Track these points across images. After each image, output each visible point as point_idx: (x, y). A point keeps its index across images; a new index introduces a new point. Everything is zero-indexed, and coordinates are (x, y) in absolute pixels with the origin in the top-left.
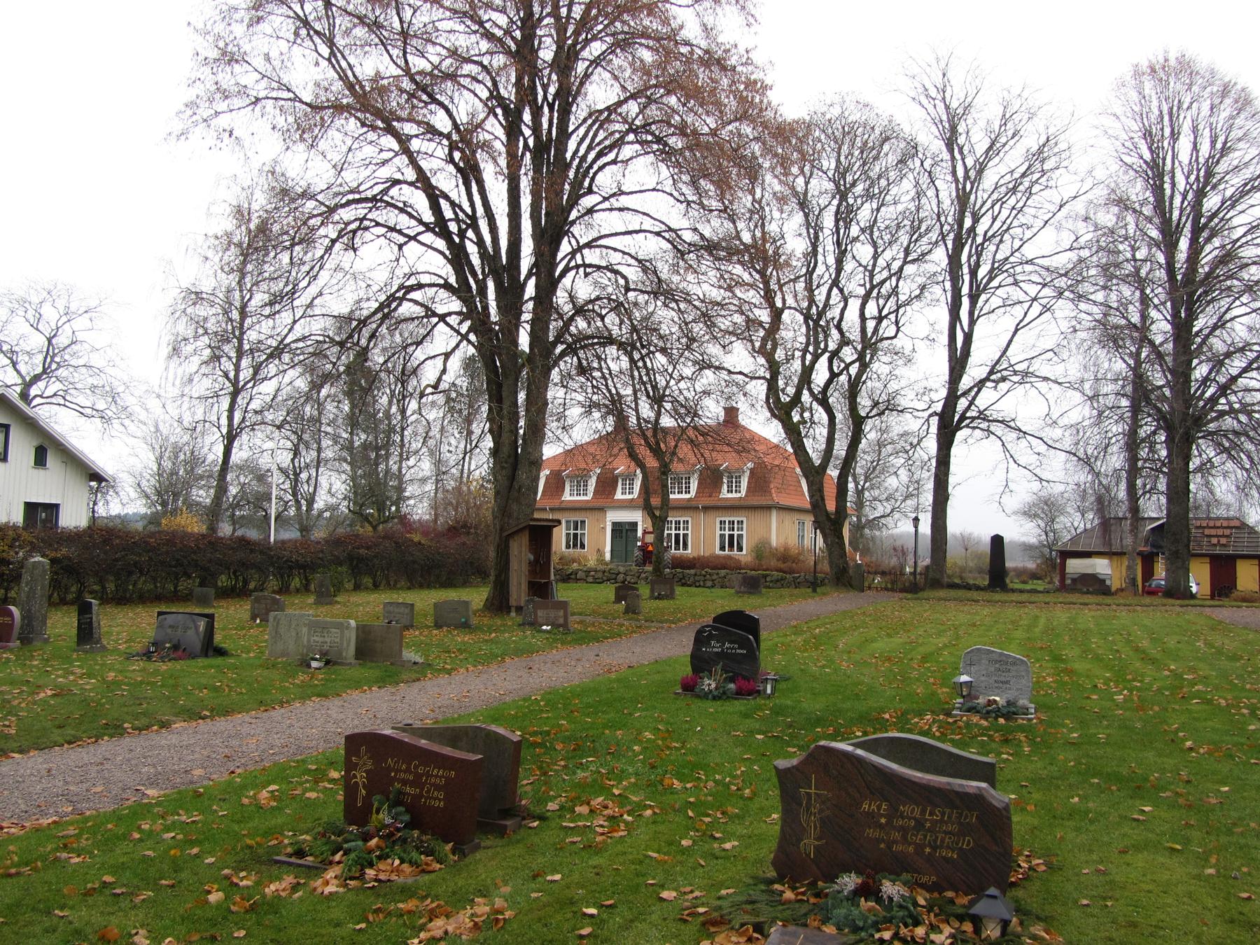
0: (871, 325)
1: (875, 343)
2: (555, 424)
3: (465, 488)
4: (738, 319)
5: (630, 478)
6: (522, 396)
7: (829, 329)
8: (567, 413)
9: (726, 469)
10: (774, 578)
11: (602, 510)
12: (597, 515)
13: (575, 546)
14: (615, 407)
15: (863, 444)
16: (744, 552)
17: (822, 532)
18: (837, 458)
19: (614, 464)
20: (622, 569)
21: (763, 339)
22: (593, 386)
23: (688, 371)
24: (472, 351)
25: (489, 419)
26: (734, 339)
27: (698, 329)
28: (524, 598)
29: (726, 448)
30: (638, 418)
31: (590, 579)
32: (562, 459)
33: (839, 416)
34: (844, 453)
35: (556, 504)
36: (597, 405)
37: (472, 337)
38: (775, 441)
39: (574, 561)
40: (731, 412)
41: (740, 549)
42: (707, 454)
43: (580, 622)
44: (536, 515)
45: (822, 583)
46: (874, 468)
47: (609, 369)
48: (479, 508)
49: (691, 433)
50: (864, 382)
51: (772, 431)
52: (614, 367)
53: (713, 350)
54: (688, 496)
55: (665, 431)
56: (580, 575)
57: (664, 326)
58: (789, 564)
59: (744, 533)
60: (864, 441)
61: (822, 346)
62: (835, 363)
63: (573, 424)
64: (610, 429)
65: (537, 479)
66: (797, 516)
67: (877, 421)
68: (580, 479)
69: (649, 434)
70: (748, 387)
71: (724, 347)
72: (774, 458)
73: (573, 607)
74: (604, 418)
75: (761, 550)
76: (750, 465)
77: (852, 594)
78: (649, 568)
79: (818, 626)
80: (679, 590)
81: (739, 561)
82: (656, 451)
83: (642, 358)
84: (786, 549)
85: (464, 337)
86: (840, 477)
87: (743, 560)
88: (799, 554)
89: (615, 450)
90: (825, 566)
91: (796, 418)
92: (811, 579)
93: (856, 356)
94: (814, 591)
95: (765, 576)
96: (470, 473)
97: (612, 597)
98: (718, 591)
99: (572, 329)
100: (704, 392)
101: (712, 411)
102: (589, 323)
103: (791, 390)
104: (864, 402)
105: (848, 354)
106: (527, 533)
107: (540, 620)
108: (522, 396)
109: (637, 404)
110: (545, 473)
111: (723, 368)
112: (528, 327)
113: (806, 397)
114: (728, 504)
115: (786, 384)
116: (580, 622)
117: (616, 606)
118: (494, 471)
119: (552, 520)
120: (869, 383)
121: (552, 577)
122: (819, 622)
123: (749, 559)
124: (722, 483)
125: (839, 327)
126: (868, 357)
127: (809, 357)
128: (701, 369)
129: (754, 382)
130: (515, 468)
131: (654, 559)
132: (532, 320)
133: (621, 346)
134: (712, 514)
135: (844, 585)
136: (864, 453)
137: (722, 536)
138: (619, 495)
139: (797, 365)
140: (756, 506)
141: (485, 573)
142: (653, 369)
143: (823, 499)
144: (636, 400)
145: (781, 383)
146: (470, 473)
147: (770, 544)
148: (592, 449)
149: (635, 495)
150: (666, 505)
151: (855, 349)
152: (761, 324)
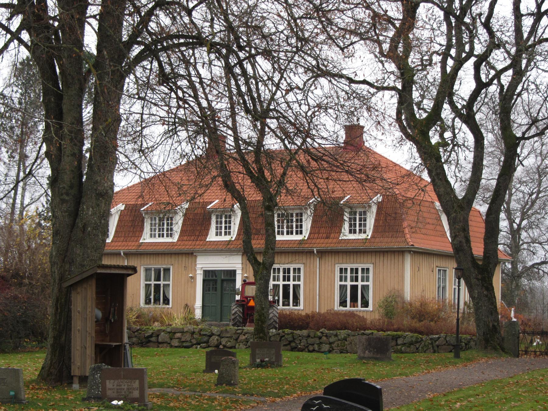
0: (527, 22)
1: (533, 46)
2: (129, 147)
3: (16, 228)
4: (362, 14)
5: (225, 214)
6: (88, 112)
7: (475, 27)
8: (146, 132)
9: (347, 204)
10: (406, 341)
11: (191, 254)
12: (184, 260)
13: (157, 300)
14: (207, 124)
15: (519, 172)
16: (370, 308)
17: (467, 283)
18: (487, 190)
19: (206, 198)
20: (215, 330)
21: (392, 40)
22: (178, 98)
23: (298, 78)
24: (24, 53)
25: (45, 139)
26: (355, 39)
27: (310, 26)
28: (90, 364)
29: (345, 177)
30: (237, 139)
31: (175, 343)
32: (138, 190)
33: (489, 138)
34: (494, 183)
35: (132, 247)
36: (184, 123)
37: (25, 36)
38: (408, 167)
39: (155, 319)
40: (354, 132)
41: (365, 304)
42: (322, 184)
43: (162, 396)
44: (106, 261)
45: (467, 347)
46: (533, 202)
47: (199, 75)
48: (34, 252)
49: (302, 158)
50: (519, 95)
51: (403, 155)
52: (204, 73)
53: (330, 53)
54: (299, 237)
55: (270, 154)
56: (163, 337)
57: (269, 24)
58: (426, 322)
59: (370, 283)
60: (519, 169)
61: (467, 48)
62: (483, 69)
63: (152, 147)
64: (199, 152)
65: (107, 215)
66: (438, 262)
67: (536, 143)
68: (164, 216)
69: (250, 159)
70: (374, 100)
71: (342, 49)
72: (407, 190)
73: (151, 377)
74: (190, 139)
75: (391, 305)
76: (379, 198)
77: (504, 360)
78: (250, 328)
79: (458, 400)
80: (287, 355)
81: (364, 319)
82: (259, 181)
83: (240, 63)
84: (423, 304)
85: (15, 36)
86: (489, 212)
87: (369, 318)
88: (439, 310)
89: (207, 180)
90: (471, 326)
91: (435, 139)
92: (453, 341)
93: (509, 62)
94: (457, 356)
95: (396, 338)
96: (23, 208)
97: (202, 364)
98: (336, 357)
99: (153, 25)
100: (319, 106)
101: (330, 129)
102: (174, 19)
103: (428, 104)
104: (519, 119)
105: (499, 59)
106: (93, 283)
107: (109, 393)
108: (88, 112)
109: (234, 122)
110: (117, 209)
111: (342, 76)
112: (95, 23)
113: (446, 112)
114: (350, 247)
115: (423, 97)
116: (162, 396)
117: (207, 376)
118: (53, 205)
119: (126, 268)
120: (525, 95)
121: (126, 340)
122: (461, 395)
123: (377, 316)
124: (343, 221)
125: (487, 25)
126: (524, 62)
127: (450, 62)
128: (317, 77)
129: (380, 94)
130: (78, 201)
131: (256, 316)
132: (101, 14)
133: (212, 47)
134: (329, 260)
135: (495, 349)
136: (521, 183)
137: (343, 288)
138: (212, 237)
139: (435, 73)
140: (387, 248)
141: (42, 334)
142: (255, 78)
143: (468, 241)
144: (233, 115)
145: (416, 95)
146: (23, 208)
147: (403, 298)
148: (176, 179)
149: (234, 234)
150: (272, 250)
151: (508, 53)
152: (390, 20)
